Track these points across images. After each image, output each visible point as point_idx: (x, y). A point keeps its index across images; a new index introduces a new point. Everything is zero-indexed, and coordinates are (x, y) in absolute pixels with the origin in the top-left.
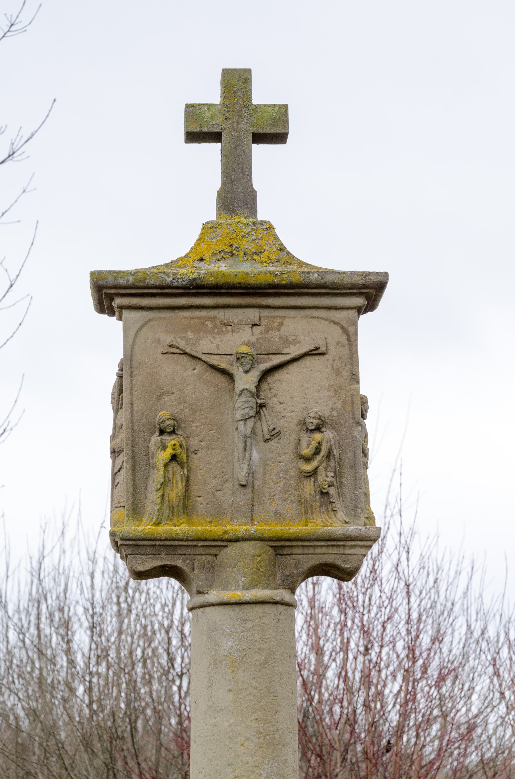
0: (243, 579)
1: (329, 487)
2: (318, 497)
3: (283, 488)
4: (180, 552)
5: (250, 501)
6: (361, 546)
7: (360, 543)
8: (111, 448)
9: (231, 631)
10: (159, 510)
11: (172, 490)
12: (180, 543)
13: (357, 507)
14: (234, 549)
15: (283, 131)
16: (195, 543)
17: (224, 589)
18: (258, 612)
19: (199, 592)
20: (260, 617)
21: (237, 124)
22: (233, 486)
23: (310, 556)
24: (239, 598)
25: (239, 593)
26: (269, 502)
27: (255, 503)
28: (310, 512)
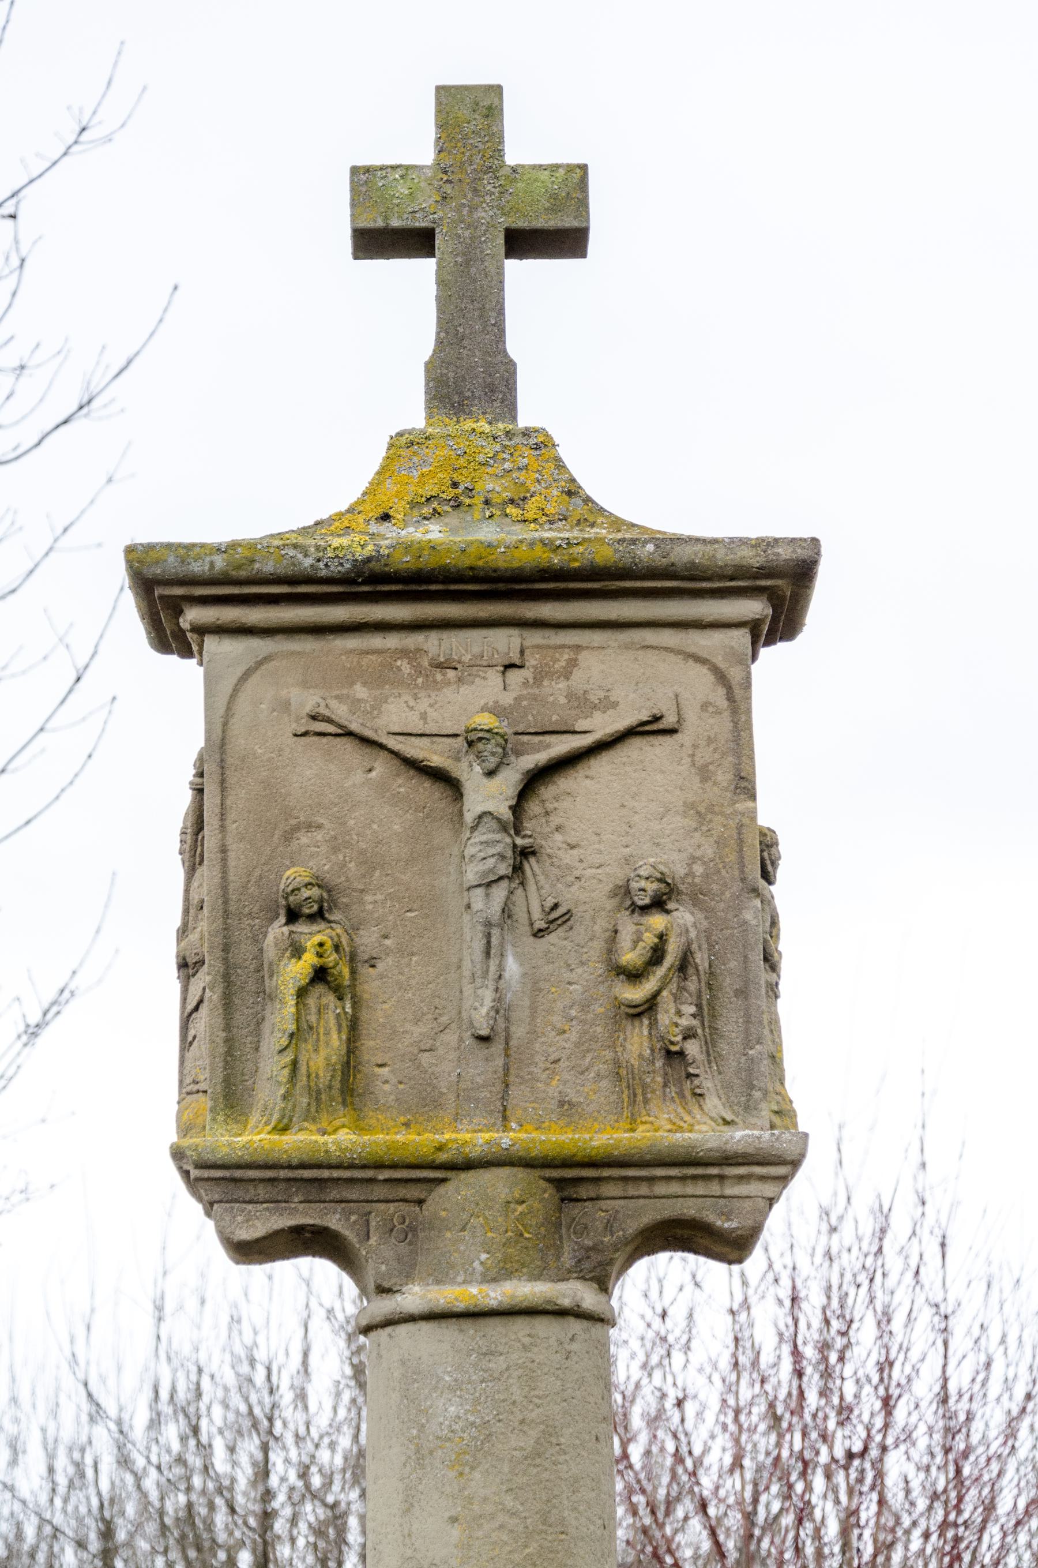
0: (484, 1256)
1: (685, 1039)
2: (659, 1064)
3: (578, 1045)
4: (334, 1194)
6: (762, 1178)
7: (758, 1170)
9: (456, 1380)
10: (284, 1098)
11: (316, 1050)
12: (336, 1174)
13: (751, 1087)
14: (462, 1189)
15: (576, 224)
16: (369, 1174)
17: (438, 1282)
18: (520, 1335)
19: (383, 1290)
20: (524, 1346)
21: (473, 215)
22: (461, 1040)
23: (642, 1201)
24: (473, 1302)
25: (474, 1290)
27: (512, 1079)
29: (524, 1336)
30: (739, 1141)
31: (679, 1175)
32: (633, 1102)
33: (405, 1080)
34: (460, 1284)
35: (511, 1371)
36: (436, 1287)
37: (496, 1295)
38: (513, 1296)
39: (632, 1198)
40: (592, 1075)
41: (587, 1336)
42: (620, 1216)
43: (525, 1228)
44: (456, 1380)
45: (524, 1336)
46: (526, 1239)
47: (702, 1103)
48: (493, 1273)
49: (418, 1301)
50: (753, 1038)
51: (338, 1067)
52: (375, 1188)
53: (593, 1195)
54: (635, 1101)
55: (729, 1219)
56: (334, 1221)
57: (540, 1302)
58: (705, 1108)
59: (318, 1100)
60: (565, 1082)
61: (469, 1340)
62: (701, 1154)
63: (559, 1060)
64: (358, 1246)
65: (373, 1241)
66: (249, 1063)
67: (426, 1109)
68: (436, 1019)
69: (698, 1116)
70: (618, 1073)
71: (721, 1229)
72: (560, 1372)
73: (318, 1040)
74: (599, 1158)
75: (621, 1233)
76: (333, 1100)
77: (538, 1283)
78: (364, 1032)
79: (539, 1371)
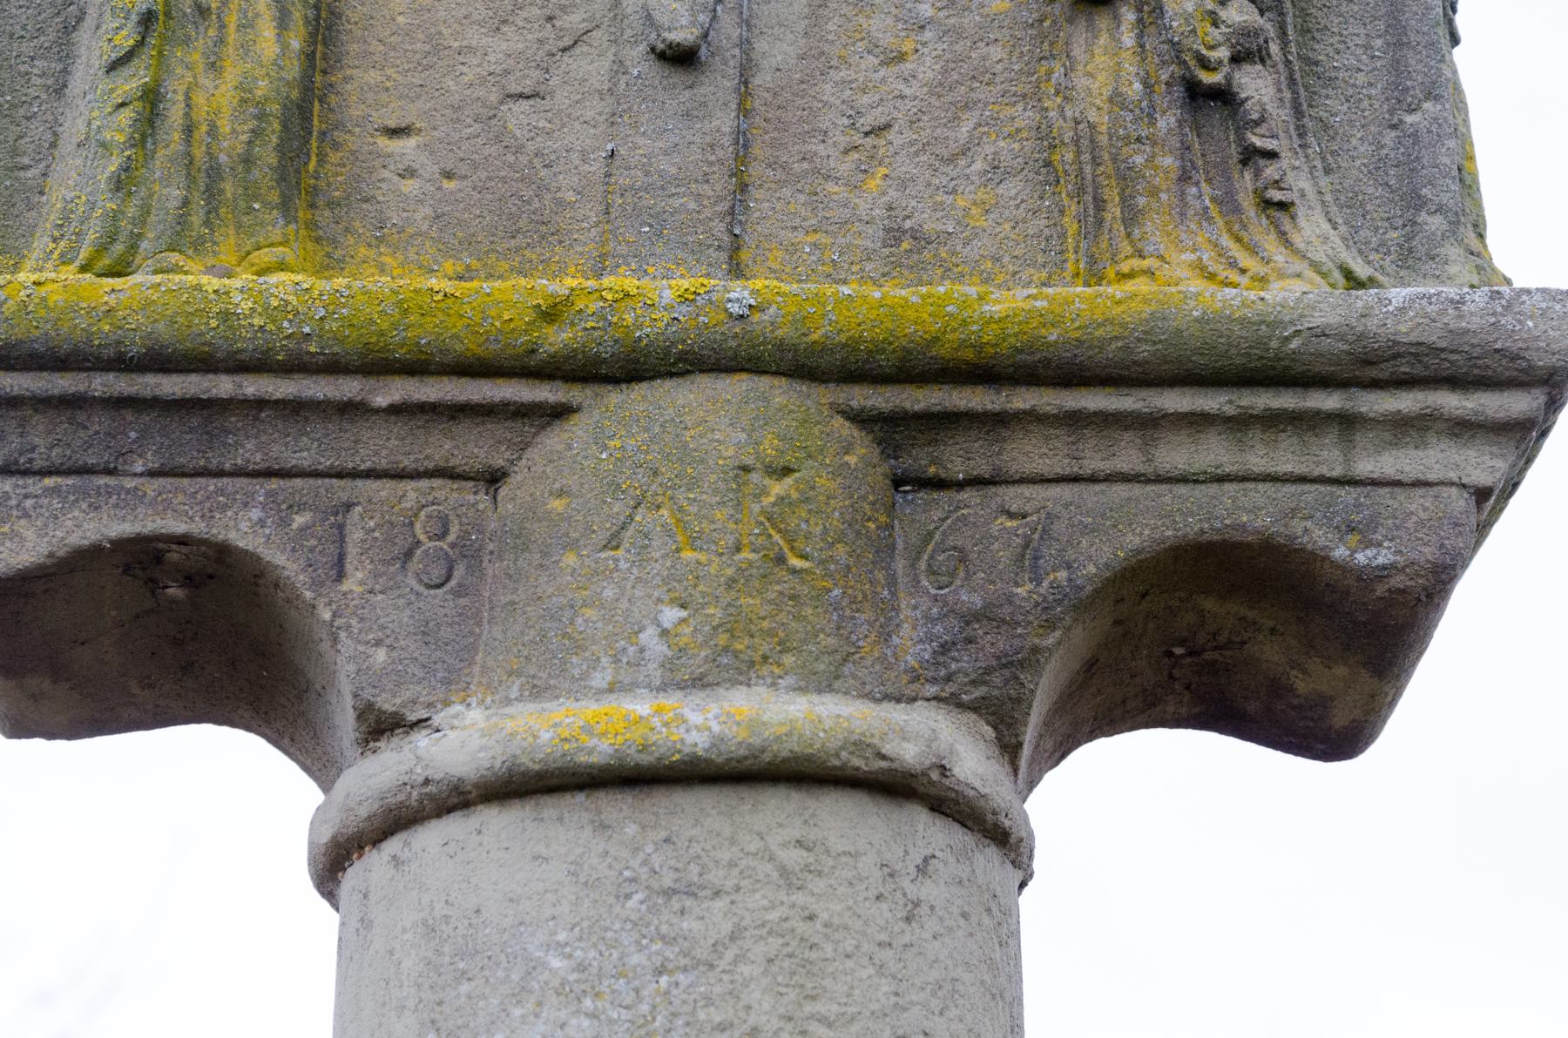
0: (670, 615)
1: (1236, 60)
2: (1166, 122)
3: (937, 89)
4: (249, 452)
5: (726, 152)
6: (1463, 428)
7: (1451, 402)
8: (311, 843)
9: (582, 967)
10: (119, 184)
11: (214, 67)
12: (252, 386)
13: (1416, 202)
14: (614, 423)
16: (348, 388)
17: (537, 692)
18: (774, 841)
19: (380, 726)
20: (784, 872)
22: (620, 66)
23: (1120, 491)
24: (636, 735)
25: (641, 706)
26: (845, 166)
27: (756, 170)
28: (1114, 211)
29: (784, 845)
30: (1402, 310)
31: (1230, 410)
32: (1094, 223)
33: (463, 169)
34: (600, 693)
35: (748, 944)
36: (532, 707)
37: (703, 722)
38: (754, 724)
39: (1093, 479)
40: (978, 166)
41: (963, 871)
42: (1059, 527)
43: (791, 542)
44: (582, 967)
45: (784, 845)
46: (794, 571)
47: (1287, 225)
48: (698, 660)
49: (476, 741)
50: (1415, 83)
51: (274, 108)
52: (366, 435)
53: (983, 468)
54: (1100, 222)
55: (1367, 544)
56: (244, 526)
57: (832, 745)
58: (1297, 239)
59: (212, 193)
60: (903, 184)
61: (624, 854)
62: (1294, 344)
63: (888, 126)
64: (308, 595)
65: (352, 584)
66: (35, 123)
67: (520, 241)
68: (550, 19)
69: (1280, 258)
70: (1048, 164)
71: (1344, 568)
72: (887, 955)
73: (221, 41)
74: (1004, 349)
75: (1062, 575)
76: (256, 198)
77: (828, 699)
78: (354, 47)
79: (829, 949)
